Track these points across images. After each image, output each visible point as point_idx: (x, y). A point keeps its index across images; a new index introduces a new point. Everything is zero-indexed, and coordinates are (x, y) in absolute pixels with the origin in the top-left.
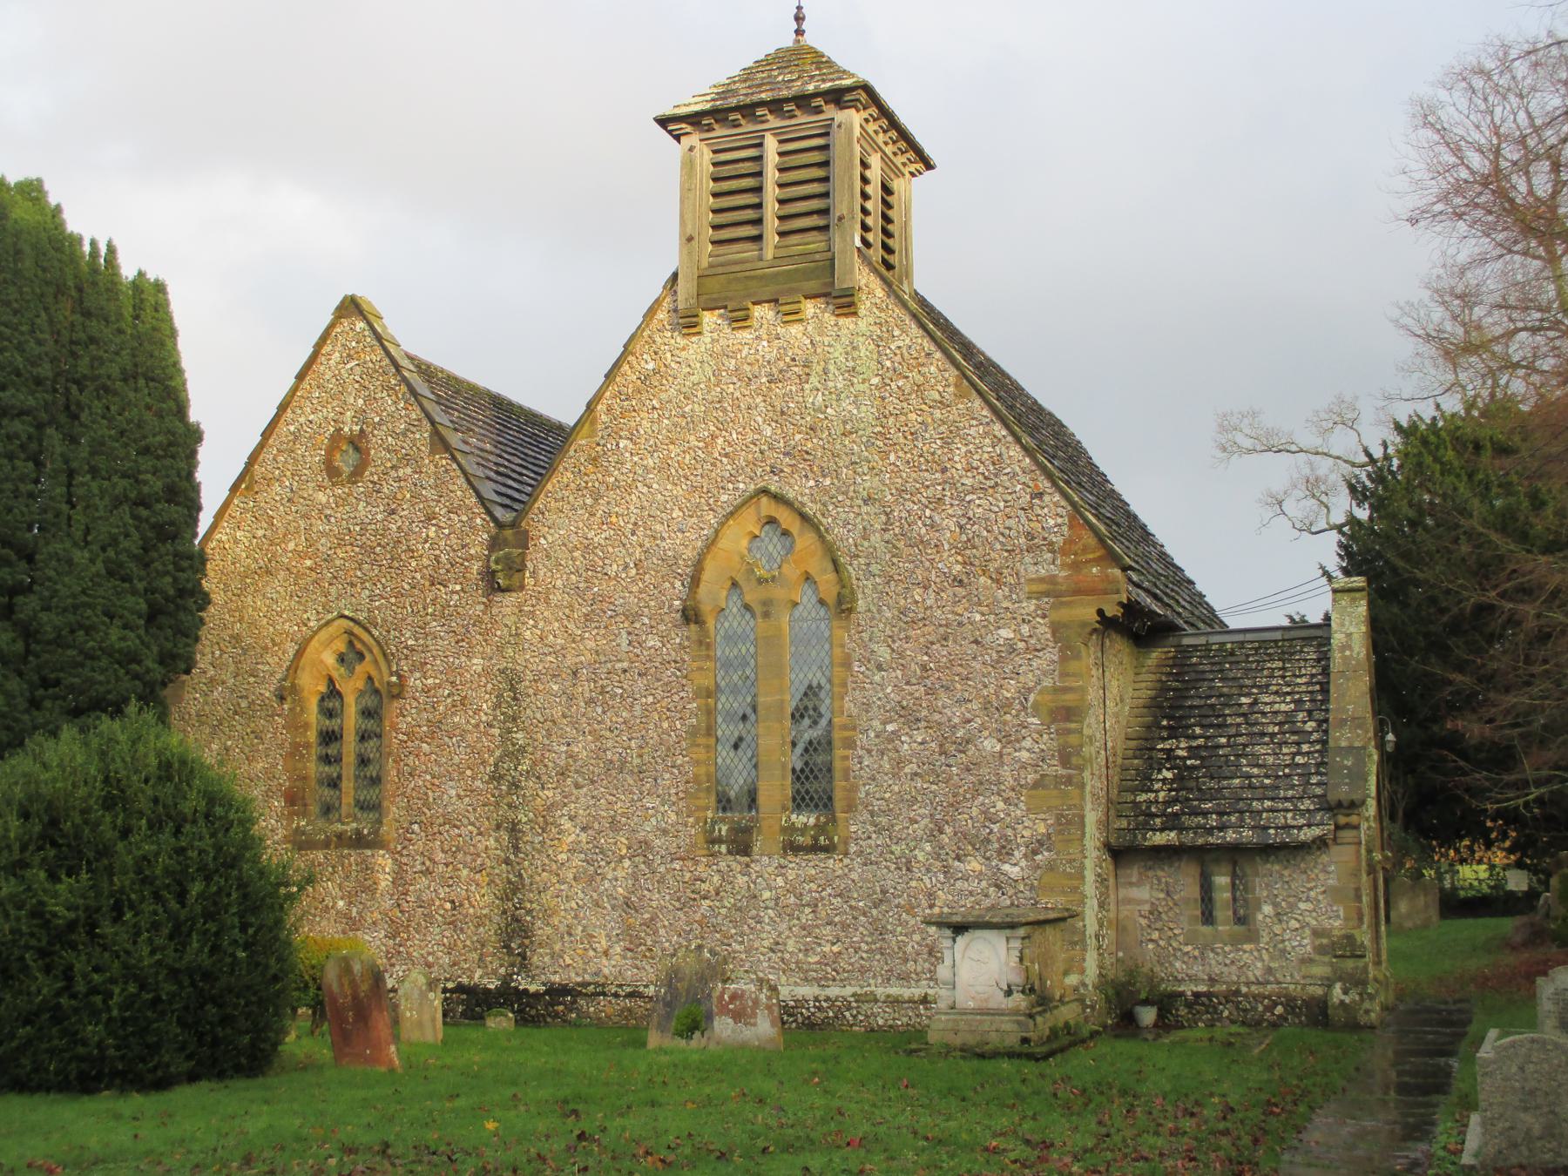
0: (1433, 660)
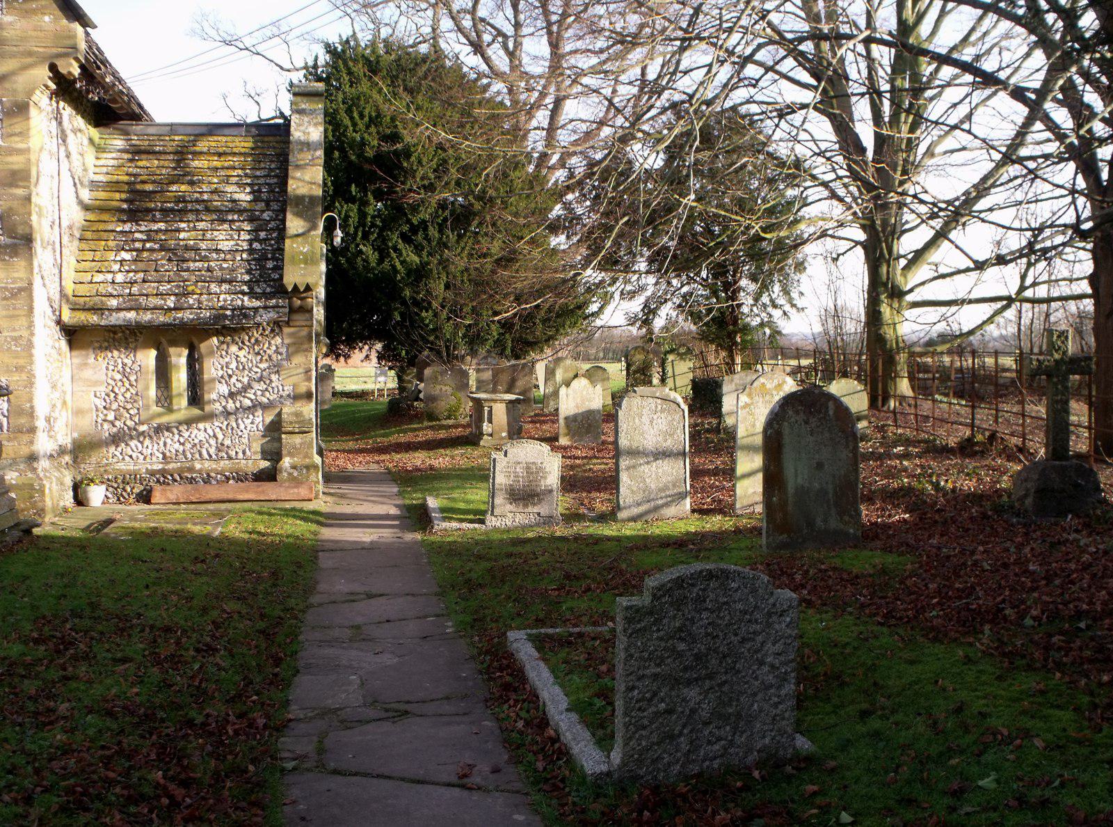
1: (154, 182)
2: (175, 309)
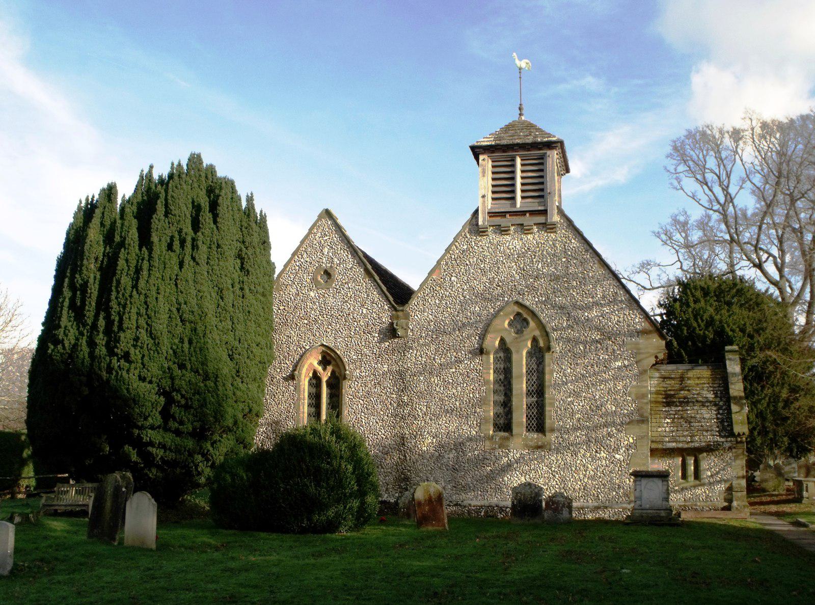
0: (105, 378)
1: (674, 390)
2: (691, 442)
